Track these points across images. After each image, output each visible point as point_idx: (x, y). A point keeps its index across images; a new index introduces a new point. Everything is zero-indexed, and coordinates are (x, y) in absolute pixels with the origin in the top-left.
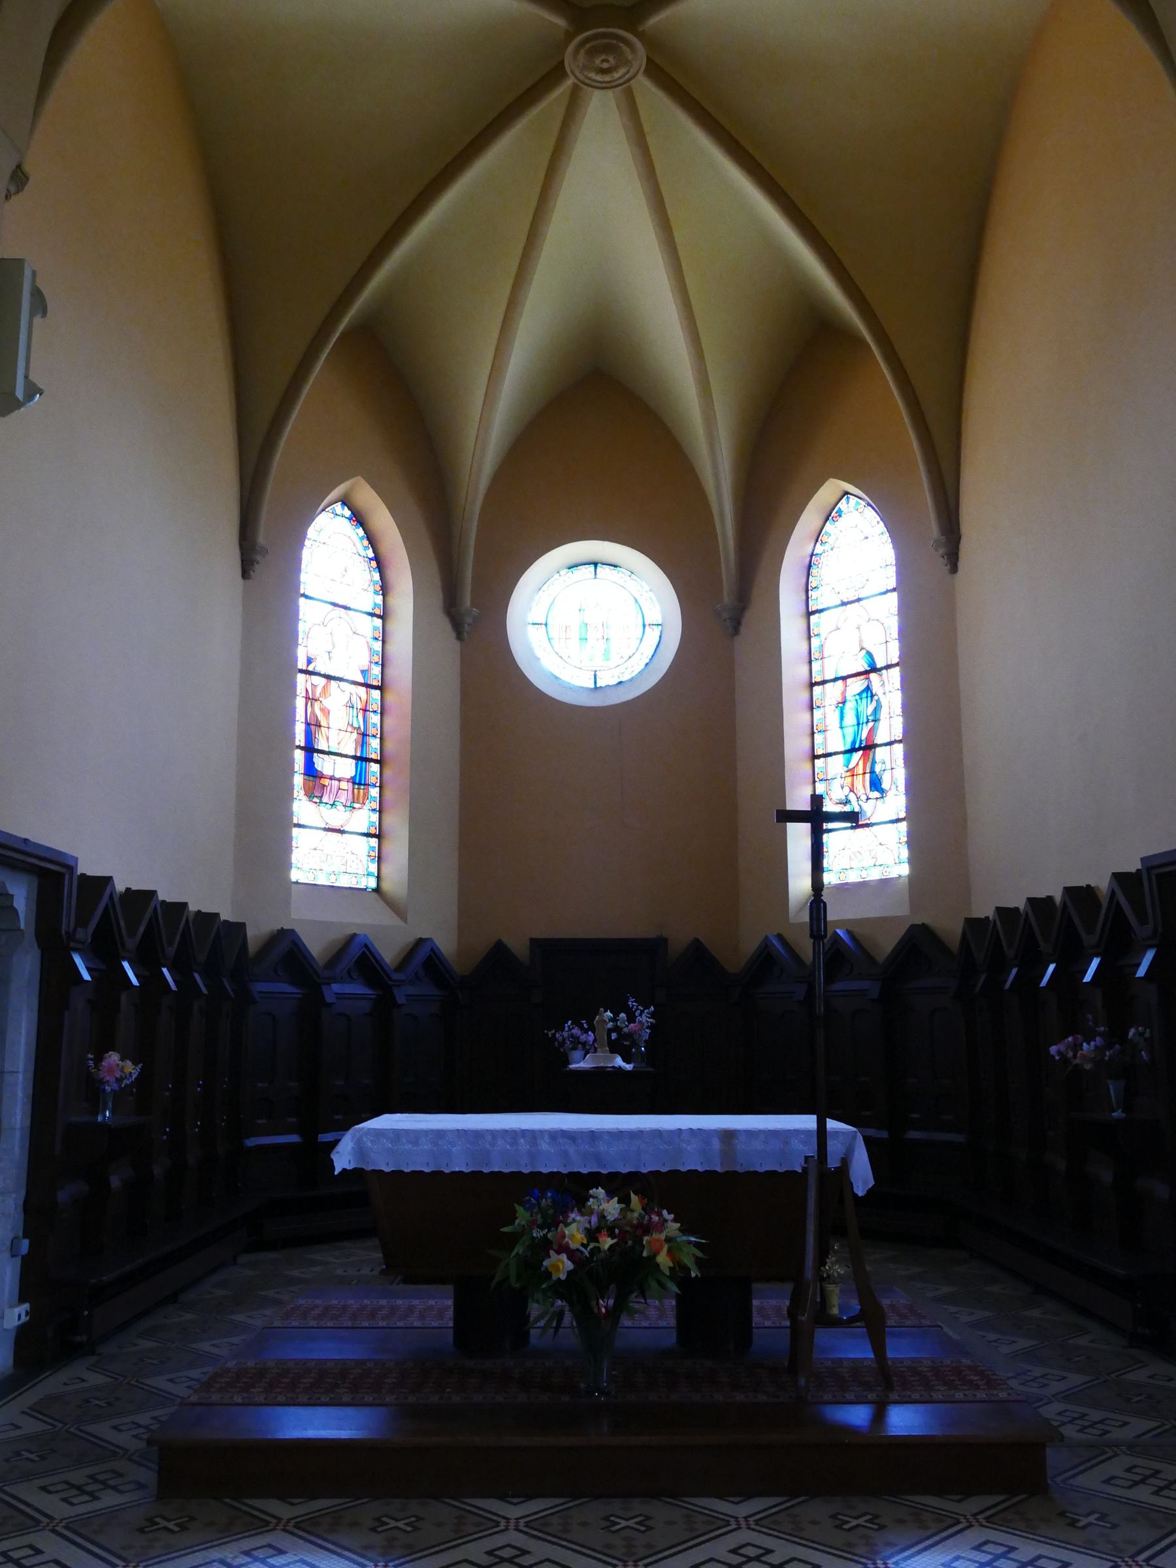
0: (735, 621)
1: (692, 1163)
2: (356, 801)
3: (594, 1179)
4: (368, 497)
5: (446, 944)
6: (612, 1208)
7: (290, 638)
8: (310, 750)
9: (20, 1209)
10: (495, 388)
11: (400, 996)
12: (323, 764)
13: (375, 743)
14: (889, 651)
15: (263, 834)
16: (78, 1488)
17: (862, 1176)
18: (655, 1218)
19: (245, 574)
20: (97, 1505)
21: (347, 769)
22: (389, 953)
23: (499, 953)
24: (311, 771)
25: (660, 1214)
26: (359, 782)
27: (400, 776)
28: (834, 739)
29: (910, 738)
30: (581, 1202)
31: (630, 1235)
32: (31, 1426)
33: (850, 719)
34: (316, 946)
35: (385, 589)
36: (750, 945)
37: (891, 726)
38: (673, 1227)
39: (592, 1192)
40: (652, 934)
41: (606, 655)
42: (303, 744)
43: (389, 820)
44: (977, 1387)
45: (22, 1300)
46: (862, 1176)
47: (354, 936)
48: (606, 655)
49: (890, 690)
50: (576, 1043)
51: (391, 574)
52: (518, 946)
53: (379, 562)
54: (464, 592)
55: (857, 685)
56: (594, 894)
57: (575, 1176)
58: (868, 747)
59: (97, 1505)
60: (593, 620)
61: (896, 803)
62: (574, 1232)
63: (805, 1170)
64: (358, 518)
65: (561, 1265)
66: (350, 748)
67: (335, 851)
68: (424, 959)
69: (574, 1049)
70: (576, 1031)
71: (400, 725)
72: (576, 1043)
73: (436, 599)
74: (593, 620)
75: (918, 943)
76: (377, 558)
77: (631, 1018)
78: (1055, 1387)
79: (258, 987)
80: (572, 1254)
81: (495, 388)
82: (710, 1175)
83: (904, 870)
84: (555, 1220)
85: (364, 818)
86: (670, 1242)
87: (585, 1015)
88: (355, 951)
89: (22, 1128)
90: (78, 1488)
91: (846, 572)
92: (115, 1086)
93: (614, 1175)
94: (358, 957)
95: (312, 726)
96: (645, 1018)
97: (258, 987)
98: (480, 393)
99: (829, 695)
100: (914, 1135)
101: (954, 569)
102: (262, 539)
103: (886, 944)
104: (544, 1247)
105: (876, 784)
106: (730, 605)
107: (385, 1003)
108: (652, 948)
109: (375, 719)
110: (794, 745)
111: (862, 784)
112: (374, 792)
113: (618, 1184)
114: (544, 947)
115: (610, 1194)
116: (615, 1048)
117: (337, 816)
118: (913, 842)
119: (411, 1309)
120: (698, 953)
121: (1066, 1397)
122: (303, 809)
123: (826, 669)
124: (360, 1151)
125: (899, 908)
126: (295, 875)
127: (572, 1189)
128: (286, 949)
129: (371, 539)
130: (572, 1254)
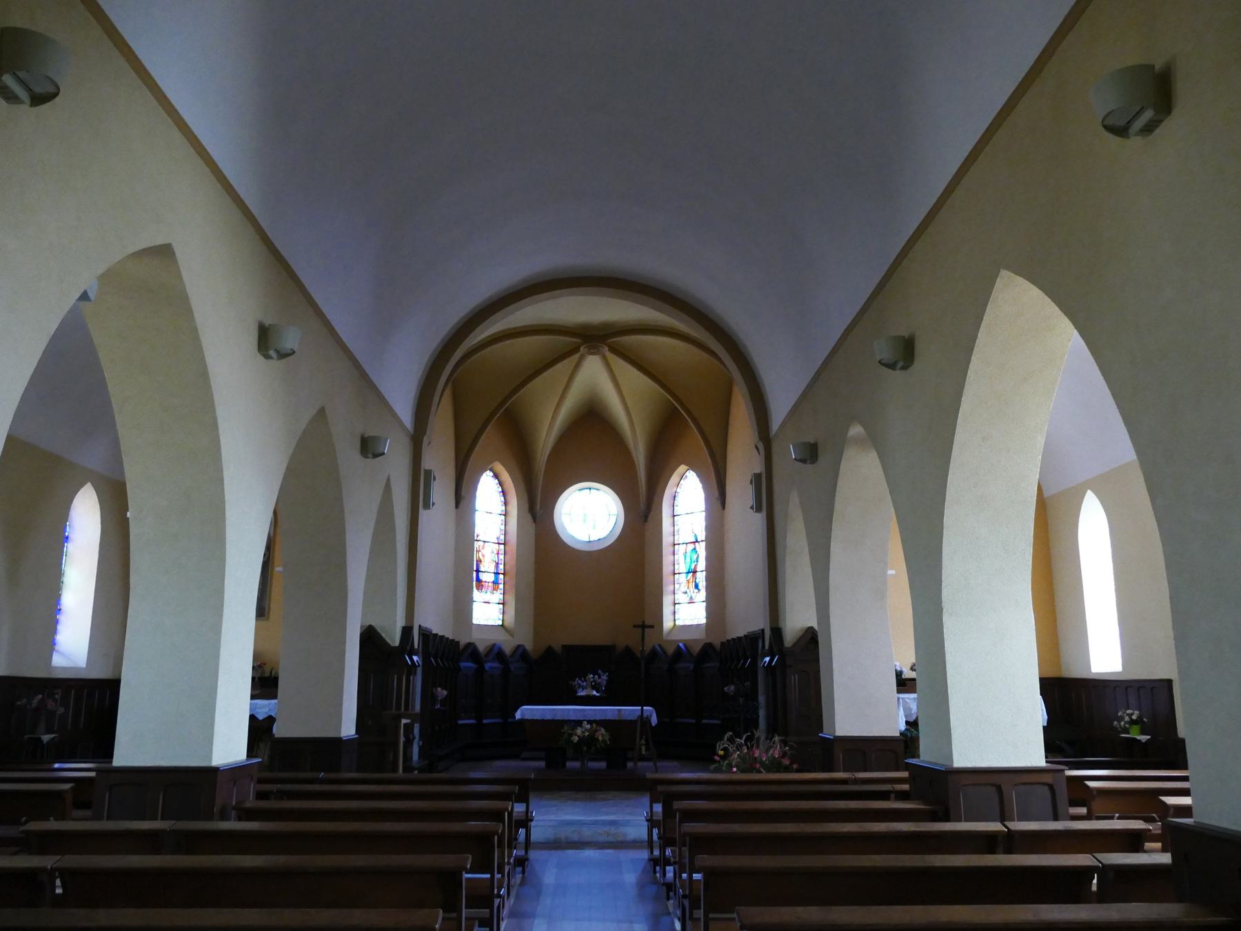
0: (646, 517)
1: (609, 717)
2: (495, 589)
4: (499, 467)
5: (529, 646)
6: (588, 726)
7: (472, 525)
8: (478, 571)
10: (550, 421)
11: (512, 667)
12: (483, 577)
13: (501, 567)
14: (702, 535)
15: (463, 606)
19: (457, 506)
21: (491, 578)
22: (508, 650)
23: (550, 650)
24: (478, 580)
26: (495, 583)
27: (512, 581)
28: (682, 567)
29: (708, 569)
31: (593, 733)
33: (688, 560)
34: (481, 648)
35: (506, 504)
36: (648, 648)
37: (702, 565)
40: (608, 643)
43: (507, 597)
46: (654, 720)
47: (494, 645)
49: (702, 548)
50: (580, 686)
51: (508, 497)
52: (557, 647)
53: (504, 493)
54: (537, 504)
55: (692, 546)
56: (587, 628)
58: (695, 572)
60: (589, 514)
61: (702, 595)
62: (579, 731)
64: (496, 476)
65: (576, 739)
66: (492, 569)
67: (488, 610)
68: (520, 652)
71: (512, 562)
72: (580, 686)
73: (526, 506)
74: (589, 514)
75: (707, 649)
76: (503, 492)
79: (463, 665)
81: (550, 421)
82: (614, 721)
83: (704, 621)
84: (574, 728)
85: (498, 596)
86: (602, 734)
87: (583, 676)
88: (496, 651)
91: (687, 501)
94: (496, 652)
95: (479, 561)
96: (605, 677)
97: (463, 665)
98: (546, 428)
99: (680, 550)
100: (704, 721)
101: (724, 508)
102: (463, 493)
103: (696, 649)
104: (571, 735)
105: (697, 586)
106: (643, 511)
107: (480, 670)
108: (609, 649)
109: (502, 557)
110: (667, 569)
111: (692, 585)
112: (501, 586)
113: (589, 722)
114: (568, 649)
116: (594, 688)
118: (708, 609)
120: (628, 650)
122: (476, 595)
123: (679, 539)
124: (522, 714)
125: (700, 636)
126: (475, 621)
127: (579, 723)
128: (471, 648)
129: (501, 484)
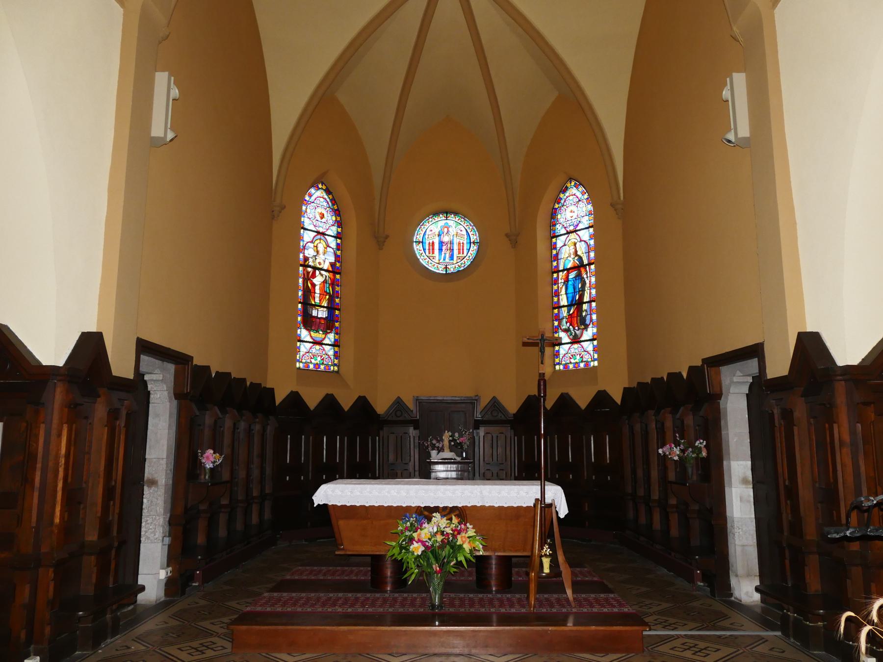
3: (436, 509)
6: (443, 522)
9: (167, 523)
16: (195, 649)
17: (563, 510)
18: (463, 526)
20: (204, 656)
25: (465, 525)
30: (429, 520)
32: (174, 623)
33: (571, 290)
34: (312, 398)
38: (471, 532)
39: (434, 514)
41: (452, 257)
42: (566, 304)
44: (614, 607)
45: (168, 566)
48: (452, 257)
57: (427, 508)
59: (204, 656)
63: (535, 505)
69: (433, 449)
70: (434, 442)
72: (434, 447)
77: (461, 436)
78: (655, 609)
80: (423, 543)
89: (166, 485)
90: (195, 649)
92: (211, 466)
93: (445, 508)
104: (411, 540)
115: (443, 516)
117: (319, 336)
119: (357, 575)
121: (660, 613)
127: (426, 513)
130: (423, 543)
